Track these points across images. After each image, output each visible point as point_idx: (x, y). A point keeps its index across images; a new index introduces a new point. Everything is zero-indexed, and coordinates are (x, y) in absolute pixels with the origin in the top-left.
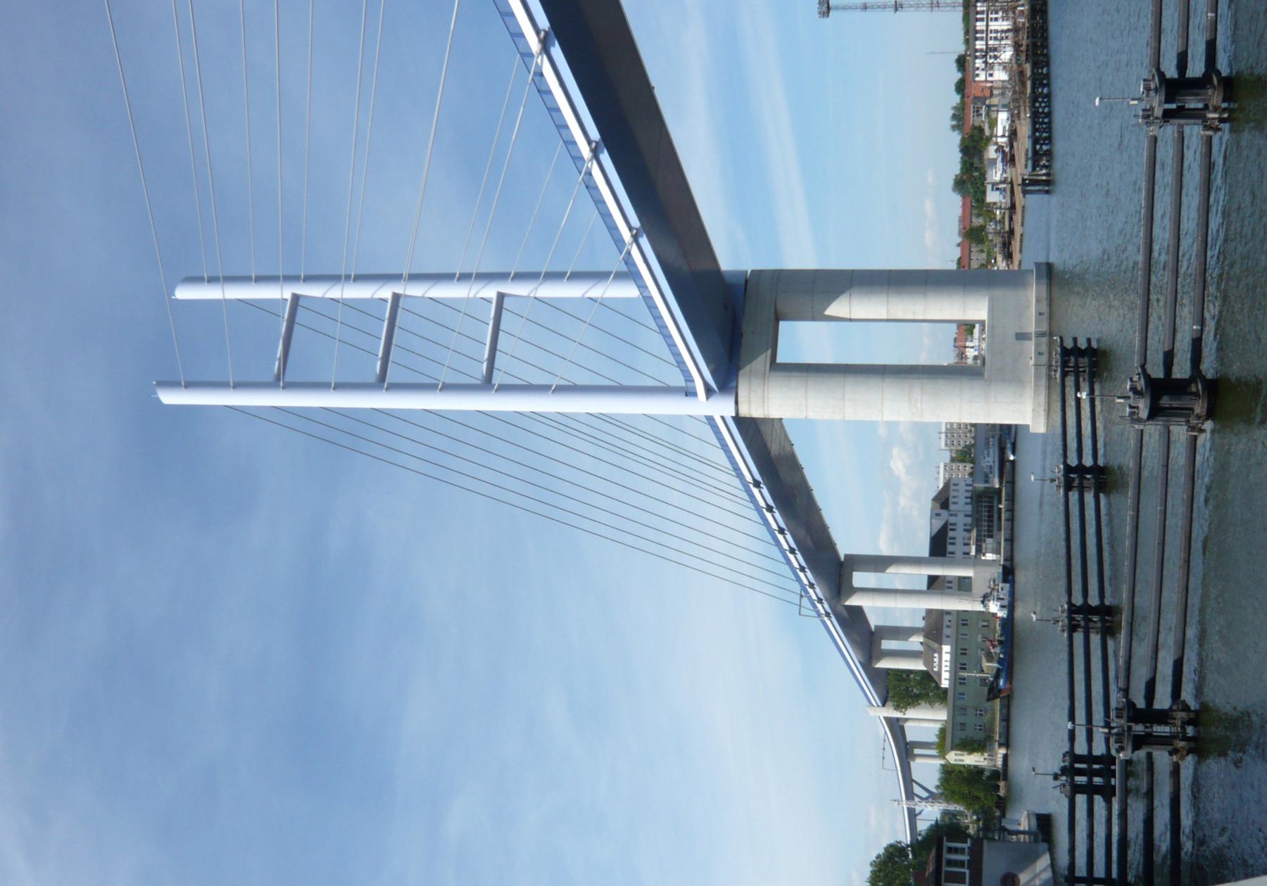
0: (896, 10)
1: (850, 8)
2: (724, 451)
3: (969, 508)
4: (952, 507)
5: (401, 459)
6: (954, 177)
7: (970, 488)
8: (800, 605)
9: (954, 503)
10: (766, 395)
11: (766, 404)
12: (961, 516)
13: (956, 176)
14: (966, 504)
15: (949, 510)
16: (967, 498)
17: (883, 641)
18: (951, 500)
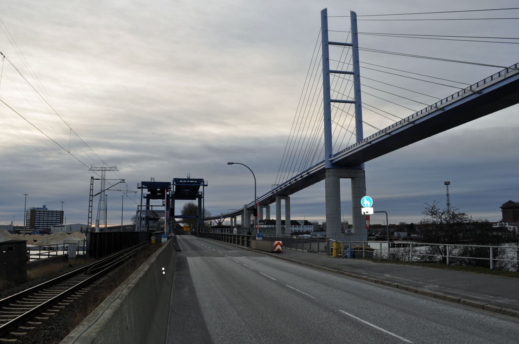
0: (447, 204)
1: (448, 191)
2: (316, 165)
3: (305, 231)
4: (305, 226)
5: (309, 78)
6: (405, 222)
7: (311, 231)
8: (275, 185)
9: (306, 227)
12: (303, 229)
14: (306, 230)
15: (304, 225)
16: (308, 230)
17: (265, 208)
18: (307, 226)
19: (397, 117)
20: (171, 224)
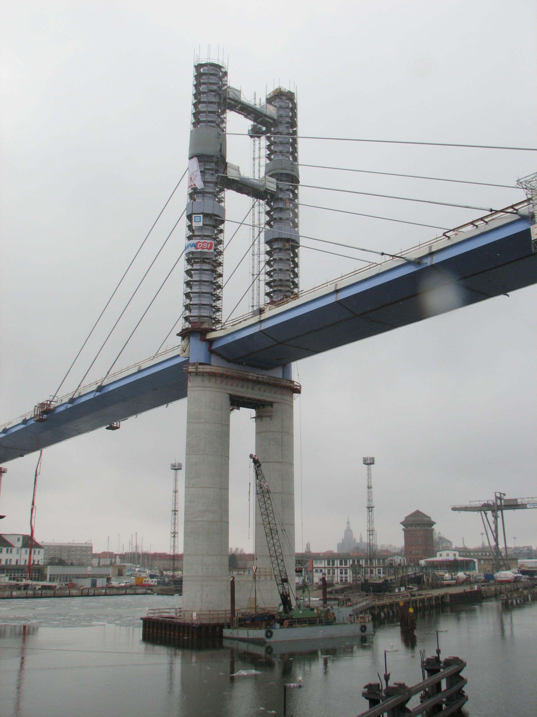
0: (368, 508)
4: (24, 550)
10: (207, 389)
11: (201, 389)
12: (18, 557)
13: (113, 553)
16: (38, 561)
19: (363, 250)
20: (382, 573)
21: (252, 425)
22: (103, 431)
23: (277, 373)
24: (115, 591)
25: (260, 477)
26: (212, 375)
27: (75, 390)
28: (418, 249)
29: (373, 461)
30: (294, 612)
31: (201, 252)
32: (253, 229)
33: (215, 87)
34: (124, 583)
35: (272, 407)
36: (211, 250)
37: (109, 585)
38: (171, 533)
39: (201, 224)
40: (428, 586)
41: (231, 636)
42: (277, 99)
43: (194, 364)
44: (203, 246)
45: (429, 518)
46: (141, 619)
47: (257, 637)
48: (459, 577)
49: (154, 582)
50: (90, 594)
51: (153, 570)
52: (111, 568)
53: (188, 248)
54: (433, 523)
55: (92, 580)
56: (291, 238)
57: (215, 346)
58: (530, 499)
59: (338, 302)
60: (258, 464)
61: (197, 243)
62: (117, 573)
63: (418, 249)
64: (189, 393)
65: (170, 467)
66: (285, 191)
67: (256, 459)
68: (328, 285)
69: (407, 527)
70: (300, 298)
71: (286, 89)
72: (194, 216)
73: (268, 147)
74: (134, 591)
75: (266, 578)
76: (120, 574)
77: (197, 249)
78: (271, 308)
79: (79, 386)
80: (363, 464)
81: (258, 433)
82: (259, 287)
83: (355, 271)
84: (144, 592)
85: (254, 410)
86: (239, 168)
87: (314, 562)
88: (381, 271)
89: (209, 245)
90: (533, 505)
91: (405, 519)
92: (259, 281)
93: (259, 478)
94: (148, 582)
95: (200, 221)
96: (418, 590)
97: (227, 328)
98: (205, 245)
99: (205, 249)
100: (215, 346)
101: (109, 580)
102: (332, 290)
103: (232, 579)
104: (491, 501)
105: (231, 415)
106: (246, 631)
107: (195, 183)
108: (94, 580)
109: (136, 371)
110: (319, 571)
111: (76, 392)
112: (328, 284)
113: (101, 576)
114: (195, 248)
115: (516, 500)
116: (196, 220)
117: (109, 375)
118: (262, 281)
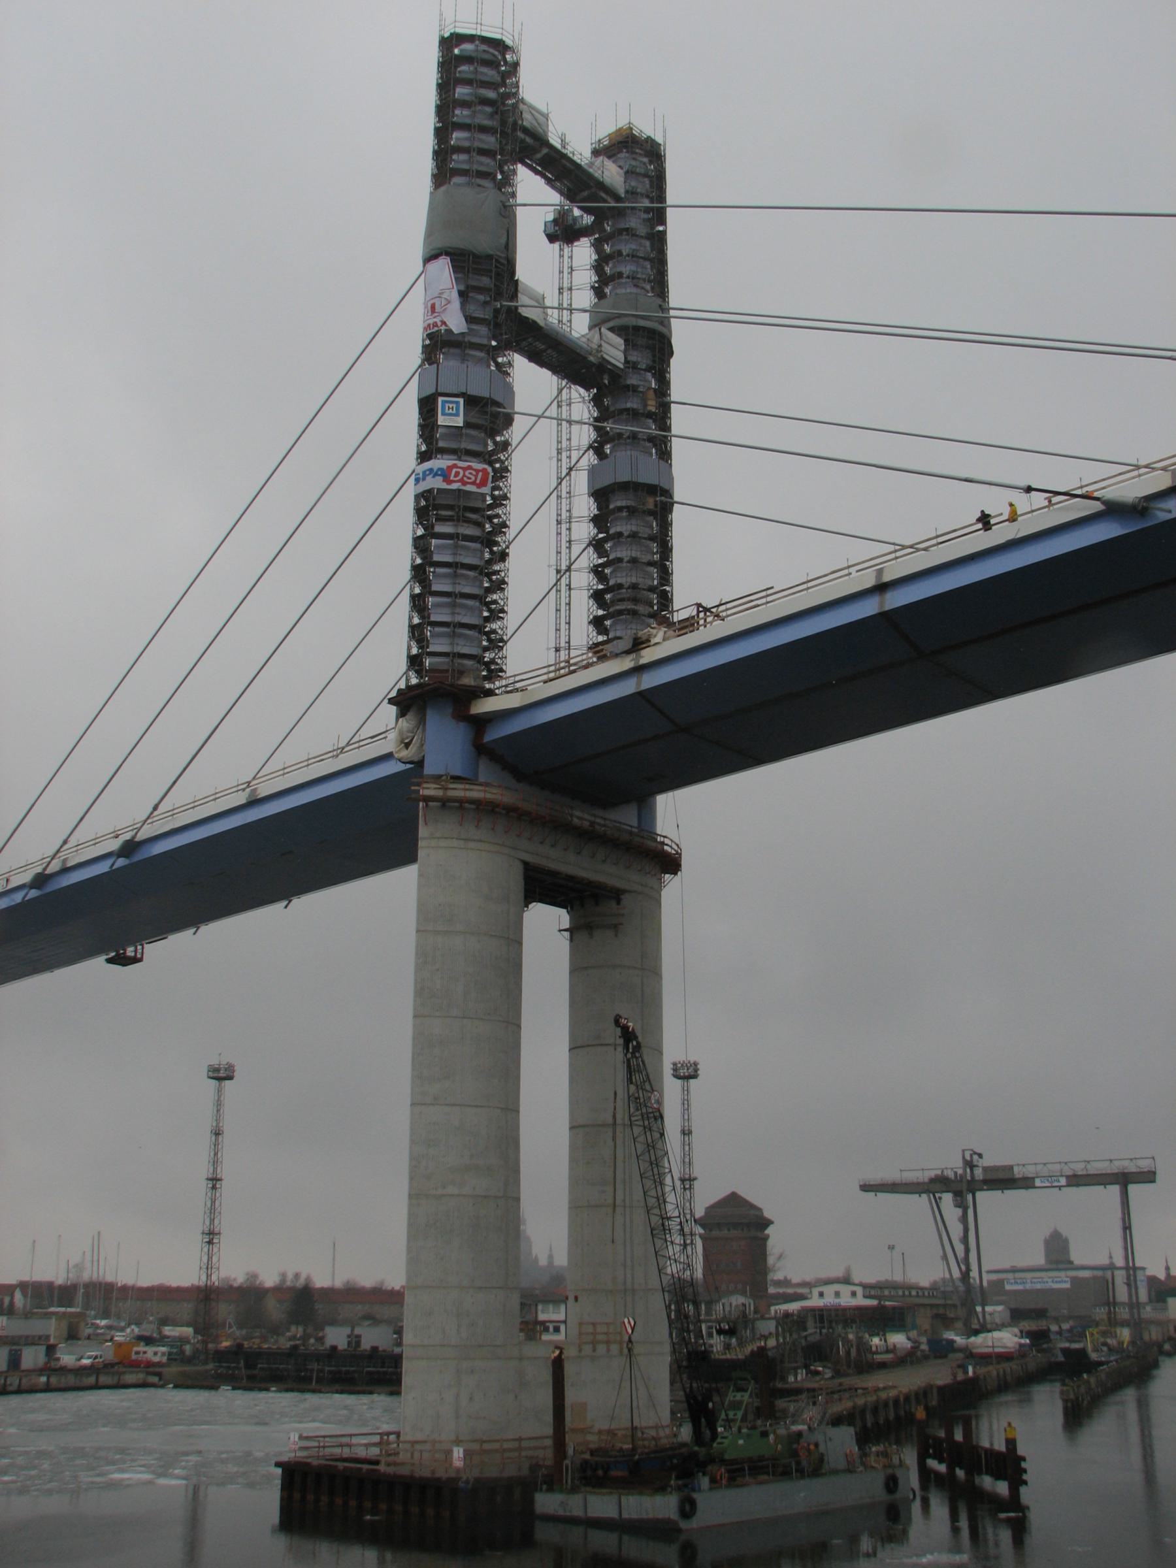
10: (472, 845)
11: (455, 843)
19: (966, 480)
21: (562, 946)
22: (98, 965)
23: (627, 817)
24: (71, 1380)
25: (636, 1077)
26: (485, 810)
27: (51, 852)
28: (1133, 478)
29: (696, 1070)
30: (726, 1441)
31: (459, 490)
32: (558, 460)
33: (491, 94)
34: (89, 1357)
35: (619, 902)
36: (484, 488)
37: (53, 1364)
38: (203, 1233)
39: (459, 421)
40: (849, 1366)
41: (561, 1512)
42: (622, 152)
43: (437, 778)
44: (464, 475)
45: (760, 1210)
46: (278, 1465)
47: (651, 1516)
48: (898, 1346)
49: (159, 1354)
50: (10, 1389)
51: (145, 1325)
52: (54, 1320)
53: (424, 479)
54: (767, 1223)
55: (11, 1351)
56: (661, 485)
57: (493, 734)
58: (1039, 1167)
59: (884, 616)
60: (635, 1043)
61: (450, 468)
62: (65, 1334)
63: (1133, 478)
64: (421, 854)
65: (204, 1072)
66: (642, 372)
67: (630, 1029)
68: (850, 574)
69: (711, 1230)
70: (993, 528)
71: (643, 130)
72: (440, 399)
73: (598, 268)
74: (116, 1379)
75: (608, 1350)
76: (72, 1335)
77: (450, 482)
78: (667, 635)
79: (65, 842)
80: (672, 1077)
81: (576, 969)
82: (569, 604)
83: (938, 537)
84: (141, 1381)
85: (564, 911)
86: (544, 298)
87: (540, 1307)
88: (1020, 535)
89: (480, 474)
90: (1050, 1179)
91: (706, 1213)
92: (570, 589)
93: (634, 1080)
94: (146, 1355)
95: (457, 415)
96: (833, 1377)
97: (529, 688)
98: (470, 473)
99: (468, 486)
100: (493, 734)
101: (51, 1349)
102: (870, 582)
103: (557, 1352)
104: (949, 1171)
105: (525, 914)
106: (615, 1498)
107: (445, 320)
108: (16, 1351)
109: (243, 801)
110: (551, 1329)
111: (53, 857)
112: (853, 570)
113: (32, 1341)
114: (444, 481)
115: (1011, 1168)
116: (447, 411)
117: (156, 813)
118: (580, 589)
